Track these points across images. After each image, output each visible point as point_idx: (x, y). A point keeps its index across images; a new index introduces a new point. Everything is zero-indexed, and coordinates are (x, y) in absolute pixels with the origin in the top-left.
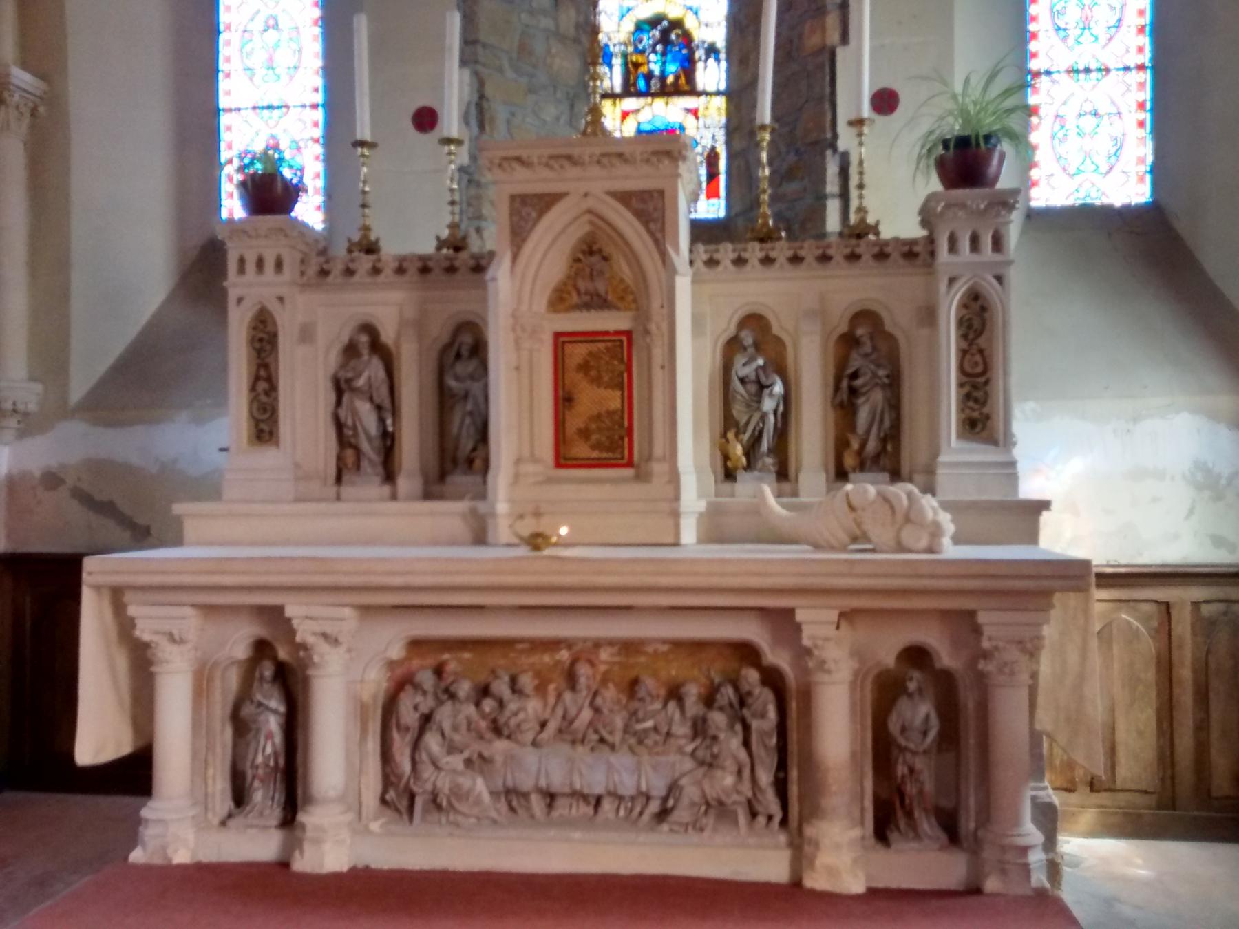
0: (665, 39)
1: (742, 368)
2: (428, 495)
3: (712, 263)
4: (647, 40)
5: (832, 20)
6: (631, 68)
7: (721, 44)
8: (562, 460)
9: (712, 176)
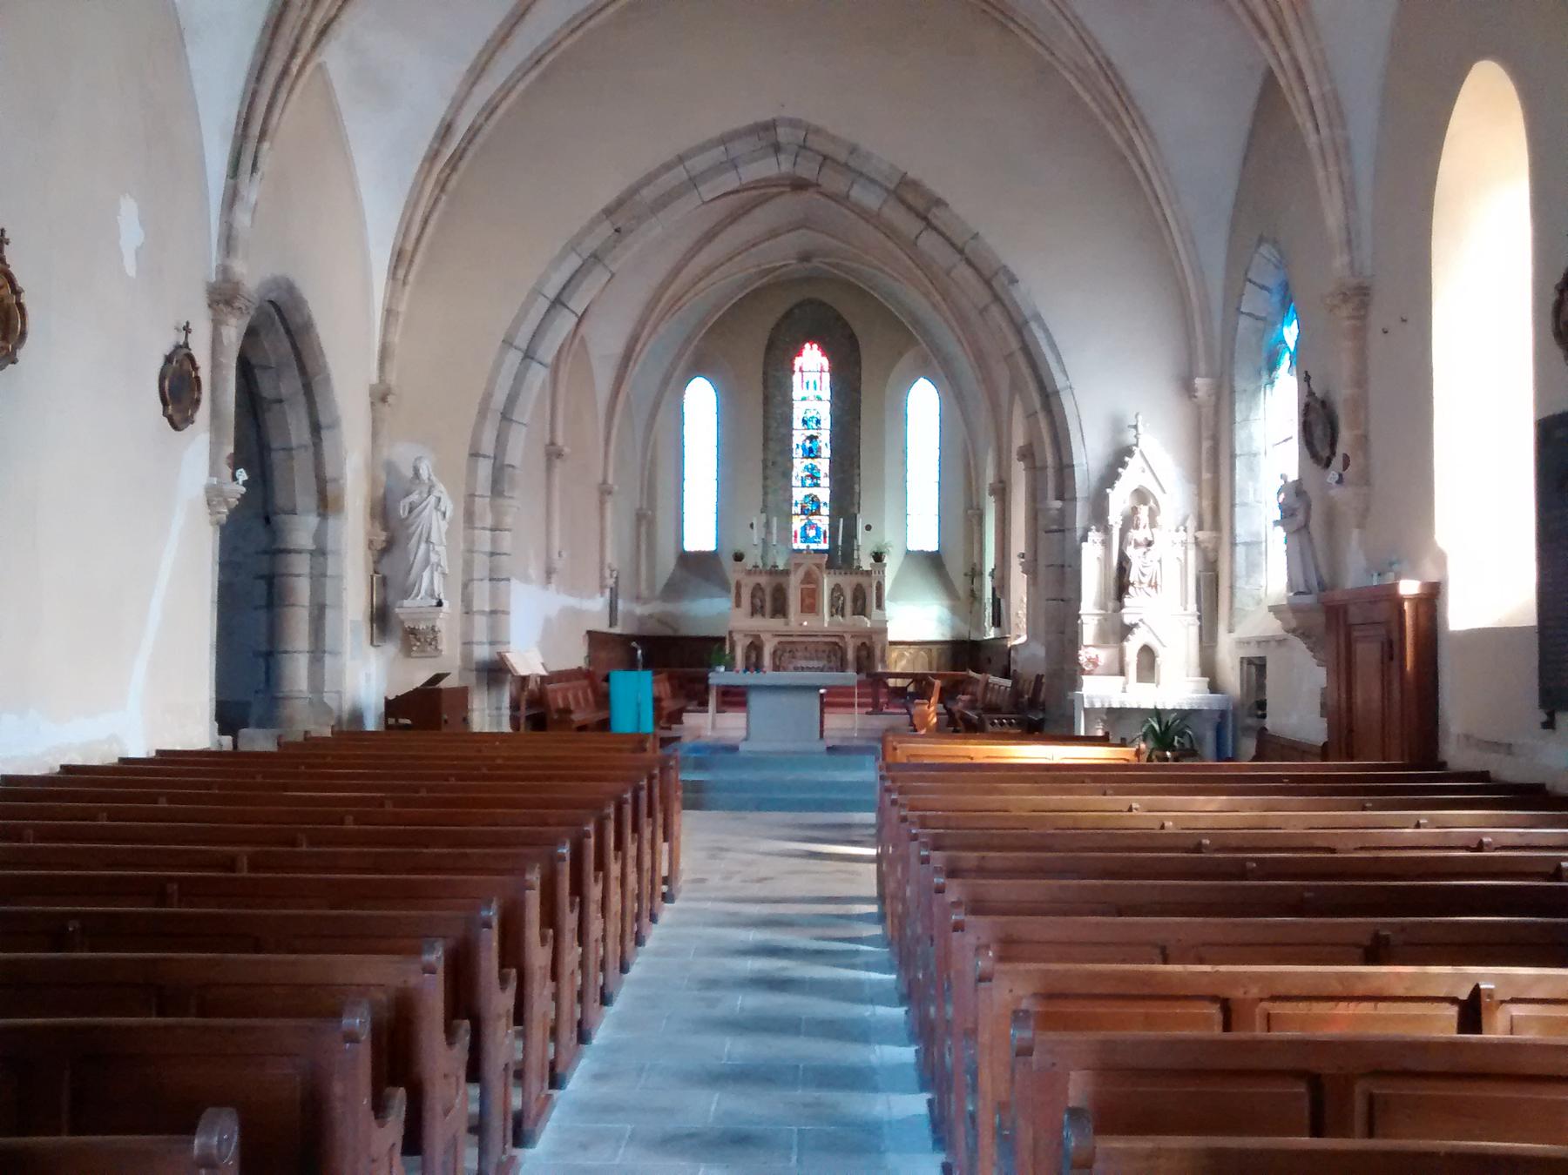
0: (813, 501)
1: (836, 594)
2: (772, 618)
3: (829, 573)
4: (807, 500)
5: (856, 506)
6: (803, 508)
7: (828, 502)
8: (802, 612)
9: (825, 537)
